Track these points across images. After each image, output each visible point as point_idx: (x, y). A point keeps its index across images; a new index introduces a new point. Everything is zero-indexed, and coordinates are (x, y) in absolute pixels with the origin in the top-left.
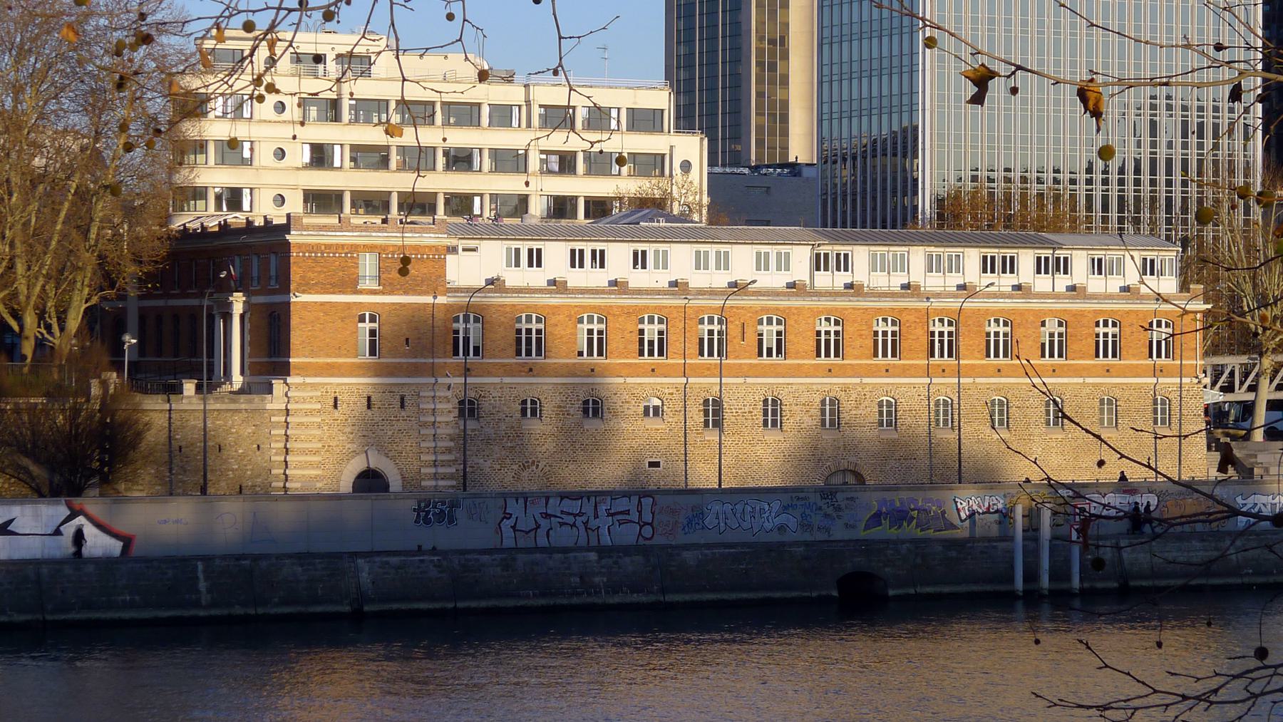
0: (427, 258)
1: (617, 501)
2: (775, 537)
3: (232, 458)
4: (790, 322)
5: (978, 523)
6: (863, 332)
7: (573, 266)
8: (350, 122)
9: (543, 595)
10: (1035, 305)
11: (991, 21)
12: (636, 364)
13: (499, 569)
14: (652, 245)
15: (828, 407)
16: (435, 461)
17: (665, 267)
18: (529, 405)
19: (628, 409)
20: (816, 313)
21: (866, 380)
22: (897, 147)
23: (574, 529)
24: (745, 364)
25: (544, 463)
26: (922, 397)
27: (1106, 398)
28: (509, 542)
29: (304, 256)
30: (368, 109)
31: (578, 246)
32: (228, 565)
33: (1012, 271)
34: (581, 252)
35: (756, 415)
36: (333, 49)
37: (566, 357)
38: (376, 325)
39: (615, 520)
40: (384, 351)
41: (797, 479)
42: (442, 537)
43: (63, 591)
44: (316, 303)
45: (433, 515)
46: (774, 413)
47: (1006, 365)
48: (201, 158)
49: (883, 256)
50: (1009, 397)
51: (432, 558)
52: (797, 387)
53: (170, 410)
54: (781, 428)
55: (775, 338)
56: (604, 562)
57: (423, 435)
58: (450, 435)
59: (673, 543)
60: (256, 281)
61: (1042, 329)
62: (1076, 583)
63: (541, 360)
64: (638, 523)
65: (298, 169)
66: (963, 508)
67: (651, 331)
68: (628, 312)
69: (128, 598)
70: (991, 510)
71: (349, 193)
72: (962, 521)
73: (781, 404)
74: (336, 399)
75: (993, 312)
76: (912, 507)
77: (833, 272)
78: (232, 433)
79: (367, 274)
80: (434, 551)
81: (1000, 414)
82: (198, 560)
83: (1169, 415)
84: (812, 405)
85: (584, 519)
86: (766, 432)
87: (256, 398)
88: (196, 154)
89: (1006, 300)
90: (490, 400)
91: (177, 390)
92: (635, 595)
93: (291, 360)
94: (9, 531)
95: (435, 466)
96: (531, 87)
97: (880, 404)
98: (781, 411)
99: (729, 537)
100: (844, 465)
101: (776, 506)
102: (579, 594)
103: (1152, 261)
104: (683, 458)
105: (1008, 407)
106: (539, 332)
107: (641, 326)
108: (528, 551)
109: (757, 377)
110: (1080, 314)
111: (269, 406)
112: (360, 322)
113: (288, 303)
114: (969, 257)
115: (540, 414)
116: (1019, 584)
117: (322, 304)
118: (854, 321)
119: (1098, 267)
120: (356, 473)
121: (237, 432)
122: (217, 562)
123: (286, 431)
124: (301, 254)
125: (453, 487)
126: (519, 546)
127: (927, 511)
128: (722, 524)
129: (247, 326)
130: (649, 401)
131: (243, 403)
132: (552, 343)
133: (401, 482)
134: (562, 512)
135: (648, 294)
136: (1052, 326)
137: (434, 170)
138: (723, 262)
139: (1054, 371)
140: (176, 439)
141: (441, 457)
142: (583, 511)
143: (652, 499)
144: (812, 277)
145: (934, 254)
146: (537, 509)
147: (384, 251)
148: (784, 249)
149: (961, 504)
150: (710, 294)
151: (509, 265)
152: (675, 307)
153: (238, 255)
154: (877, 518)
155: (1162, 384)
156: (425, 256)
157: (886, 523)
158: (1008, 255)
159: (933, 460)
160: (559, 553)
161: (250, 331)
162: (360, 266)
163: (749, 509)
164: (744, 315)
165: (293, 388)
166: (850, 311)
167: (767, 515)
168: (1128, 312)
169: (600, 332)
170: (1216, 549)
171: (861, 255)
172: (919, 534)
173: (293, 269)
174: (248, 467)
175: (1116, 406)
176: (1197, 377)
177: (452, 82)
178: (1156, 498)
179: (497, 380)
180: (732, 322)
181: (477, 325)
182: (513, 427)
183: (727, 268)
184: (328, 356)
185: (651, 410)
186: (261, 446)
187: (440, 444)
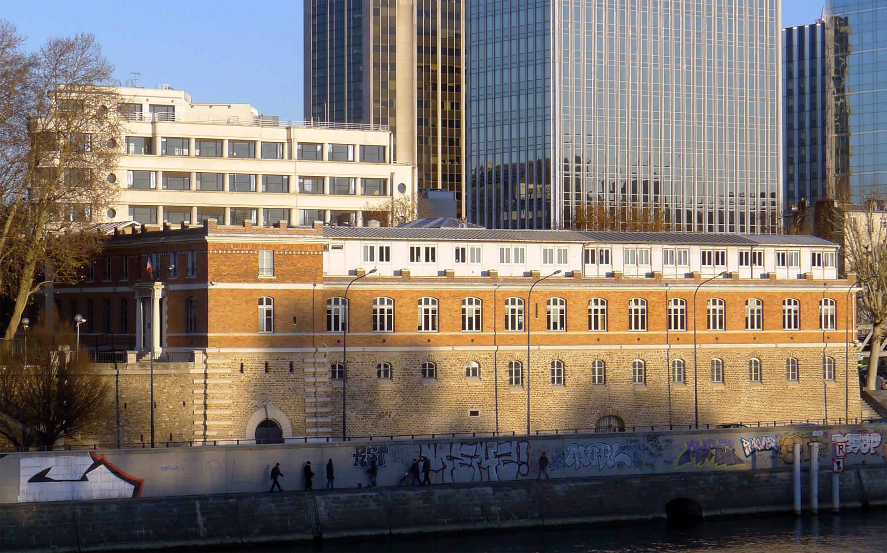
0: (309, 254)
1: (502, 445)
2: (615, 472)
3: (164, 413)
4: (570, 303)
5: (758, 459)
6: (621, 310)
7: (545, 262)
8: (162, 155)
9: (454, 522)
10: (742, 289)
11: (600, 84)
12: (460, 336)
14: (469, 244)
15: (597, 368)
18: (382, 368)
19: (455, 370)
21: (625, 347)
22: (492, 179)
23: (471, 468)
24: (538, 335)
25: (395, 413)
26: (664, 359)
27: (790, 358)
29: (218, 253)
30: (175, 145)
31: (416, 245)
32: (219, 504)
33: (723, 263)
34: (418, 249)
35: (546, 374)
36: (147, 100)
37: (410, 331)
39: (500, 460)
40: (277, 327)
41: (576, 423)
43: (93, 528)
44: (227, 289)
46: (559, 372)
47: (722, 334)
49: (633, 252)
50: (724, 359)
51: (371, 494)
53: (117, 375)
55: (559, 315)
56: (497, 494)
58: (325, 392)
60: (191, 272)
61: (746, 306)
62: (837, 504)
63: (391, 333)
66: (748, 446)
68: (454, 295)
69: (144, 532)
70: (767, 448)
71: (329, 211)
73: (564, 366)
74: (242, 365)
75: (712, 294)
76: (712, 446)
77: (598, 264)
79: (265, 267)
82: (195, 499)
83: (834, 371)
84: (587, 366)
85: (478, 460)
87: (182, 365)
89: (721, 285)
90: (355, 365)
91: (123, 359)
92: (522, 521)
93: (208, 335)
94: (47, 478)
95: (316, 417)
96: (292, 129)
97: (634, 365)
98: (564, 370)
99: (582, 473)
100: (610, 412)
101: (616, 447)
102: (480, 521)
103: (819, 255)
104: (495, 408)
105: (723, 366)
106: (389, 311)
107: (463, 307)
109: (547, 345)
110: (772, 296)
111: (192, 371)
112: (259, 304)
113: (206, 290)
114: (693, 252)
115: (391, 375)
116: (798, 506)
117: (232, 290)
118: (615, 302)
119: (782, 260)
120: (258, 423)
121: (168, 392)
122: (211, 501)
123: (205, 391)
125: (329, 433)
127: (722, 450)
128: (578, 463)
129: (165, 308)
131: (172, 368)
132: (399, 320)
133: (291, 429)
134: (462, 455)
135: (468, 282)
136: (753, 305)
137: (189, 189)
138: (520, 257)
139: (755, 338)
140: (123, 398)
141: (320, 410)
143: (527, 444)
144: (583, 268)
145: (669, 250)
146: (443, 454)
147: (277, 248)
149: (746, 443)
150: (513, 282)
152: (488, 292)
153: (155, 253)
154: (687, 455)
155: (829, 348)
156: (307, 253)
158: (707, 251)
159: (672, 407)
160: (464, 488)
161: (168, 313)
162: (259, 260)
164: (537, 298)
165: (210, 357)
166: (613, 294)
167: (609, 454)
168: (805, 294)
169: (434, 311)
171: (617, 251)
172: (717, 468)
173: (210, 263)
175: (798, 365)
176: (853, 342)
177: (236, 125)
178: (880, 436)
179: (360, 349)
182: (371, 386)
183: (523, 261)
185: (471, 371)
186: (186, 403)
187: (320, 399)
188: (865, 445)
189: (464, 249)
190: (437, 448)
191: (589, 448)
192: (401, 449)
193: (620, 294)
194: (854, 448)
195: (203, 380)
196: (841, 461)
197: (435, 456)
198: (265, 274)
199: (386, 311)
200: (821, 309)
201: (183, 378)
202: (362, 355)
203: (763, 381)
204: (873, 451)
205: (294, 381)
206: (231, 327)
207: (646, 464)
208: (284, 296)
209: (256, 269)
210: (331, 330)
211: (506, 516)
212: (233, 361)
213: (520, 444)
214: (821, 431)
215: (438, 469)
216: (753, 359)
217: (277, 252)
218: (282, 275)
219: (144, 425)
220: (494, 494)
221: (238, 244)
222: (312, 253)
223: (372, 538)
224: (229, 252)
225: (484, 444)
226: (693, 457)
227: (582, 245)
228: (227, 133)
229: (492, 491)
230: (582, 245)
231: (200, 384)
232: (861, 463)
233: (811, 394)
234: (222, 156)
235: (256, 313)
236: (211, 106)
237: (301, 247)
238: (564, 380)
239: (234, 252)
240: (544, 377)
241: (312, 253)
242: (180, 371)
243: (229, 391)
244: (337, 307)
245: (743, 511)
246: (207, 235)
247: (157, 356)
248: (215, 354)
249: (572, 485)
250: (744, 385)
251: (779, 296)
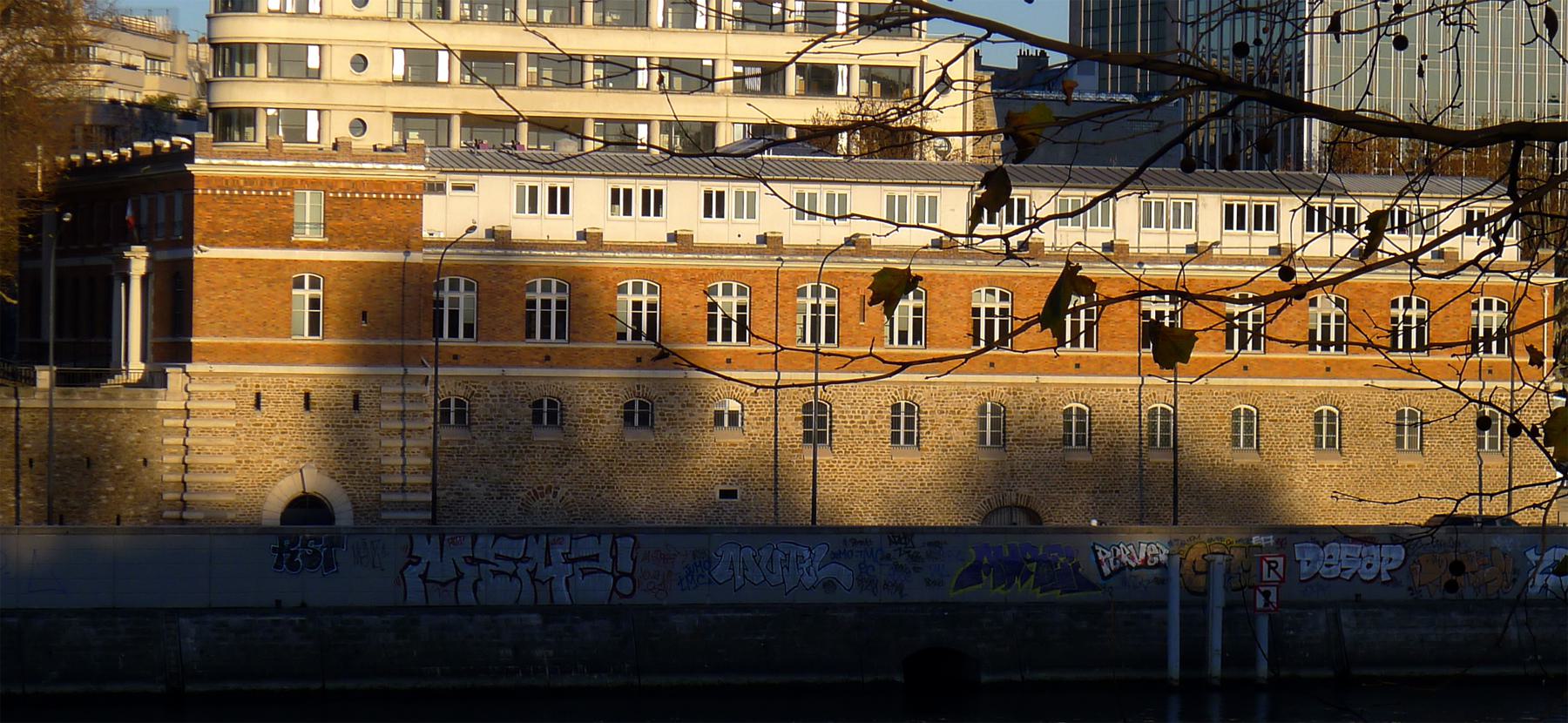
1: (580, 541)
3: (107, 477)
7: (708, 214)
16: (404, 484)
17: (752, 215)
19: (691, 415)
20: (972, 283)
23: (516, 581)
25: (566, 490)
26: (1131, 405)
27: (1406, 409)
28: (415, 597)
31: (623, 184)
33: (1270, 227)
39: (576, 568)
41: (940, 517)
44: (230, 260)
45: (302, 557)
46: (909, 423)
47: (1256, 360)
48: (249, 68)
52: (942, 387)
53: (18, 408)
54: (918, 445)
57: (386, 448)
59: (665, 603)
61: (1311, 309)
64: (612, 573)
65: (385, 84)
67: (728, 303)
68: (691, 277)
70: (1149, 564)
71: (658, 123)
74: (258, 395)
76: (1029, 557)
78: (106, 442)
79: (308, 221)
80: (303, 608)
88: (553, 80)
93: (192, 340)
101: (821, 553)
105: (1258, 420)
106: (652, 306)
111: (160, 404)
114: (1205, 205)
116: (1174, 669)
117: (240, 262)
118: (1029, 295)
124: (209, 192)
126: (431, 604)
127: (1051, 564)
134: (497, 556)
139: (1328, 369)
140: (25, 449)
142: (529, 555)
148: (928, 192)
149: (1104, 554)
151: (520, 209)
152: (762, 272)
154: (973, 573)
156: (392, 196)
157: (988, 580)
162: (295, 210)
163: (780, 555)
166: (1023, 280)
167: (805, 566)
174: (130, 490)
178: (1403, 551)
180: (847, 294)
182: (520, 439)
184: (247, 334)
185: (726, 417)
186: (150, 460)
188: (1369, 566)
189: (661, 191)
190: (445, 543)
191: (763, 552)
192: (372, 542)
193: (1039, 281)
194: (1342, 570)
195: (183, 421)
196: (1273, 590)
197: (442, 557)
198: (309, 234)
199: (983, 313)
200: (1478, 317)
201: (144, 416)
202: (503, 383)
203: (1344, 450)
204: (1386, 577)
205: (361, 426)
206: (238, 327)
208: (344, 274)
209: (288, 223)
210: (457, 337)
212: (242, 388)
213: (618, 540)
214: (1271, 537)
215: (444, 580)
216: (1325, 408)
217: (331, 195)
219: (65, 498)
221: (255, 178)
222: (400, 196)
224: (236, 192)
226: (987, 574)
227: (969, 189)
229: (540, 622)
230: (969, 189)
231: (177, 427)
232: (1354, 598)
233: (1447, 477)
234: (581, 24)
235: (287, 302)
237: (379, 185)
238: (918, 438)
239: (245, 193)
240: (876, 432)
241: (400, 196)
242: (138, 404)
243: (231, 442)
246: (193, 162)
247: (135, 377)
248: (204, 374)
250: (1300, 455)
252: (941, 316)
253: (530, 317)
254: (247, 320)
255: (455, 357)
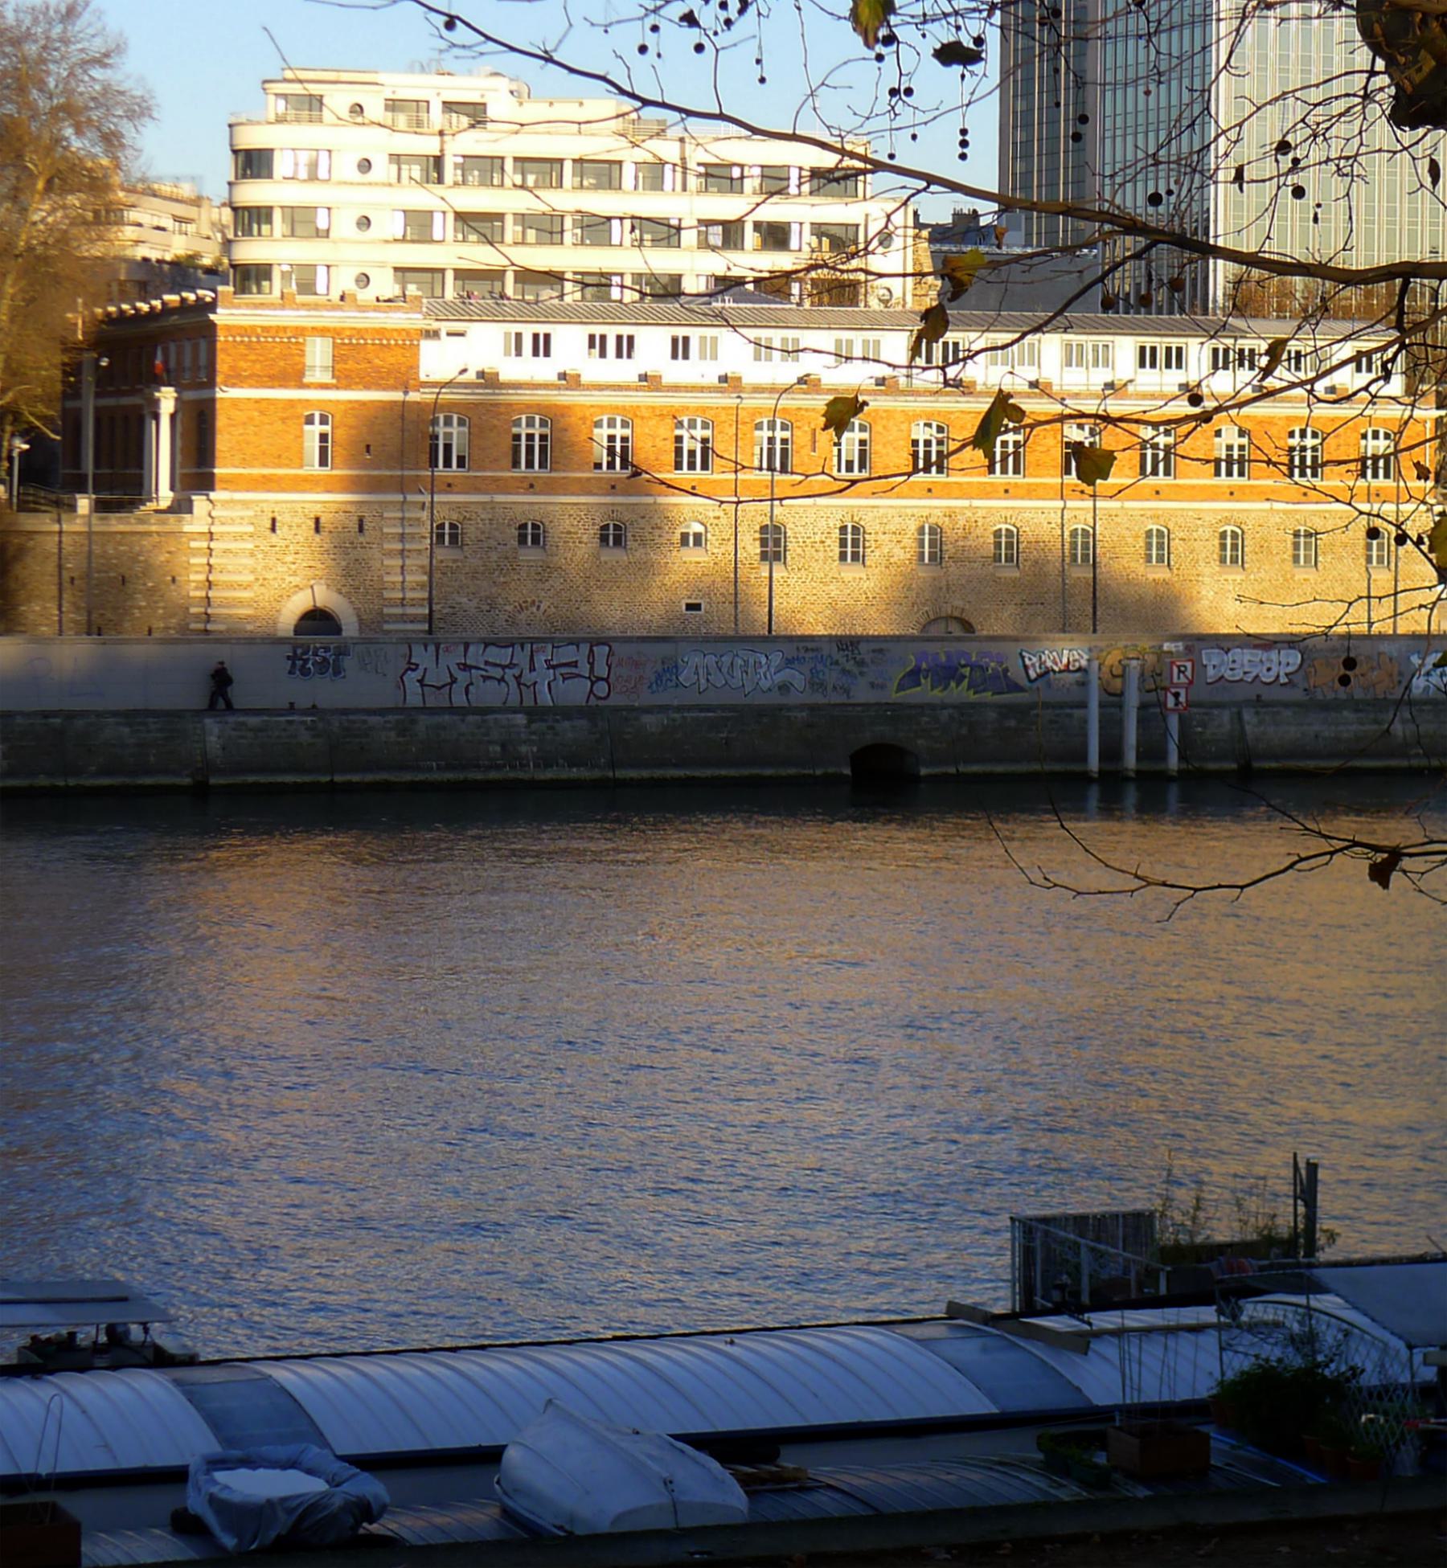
2: (776, 699)
4: (877, 428)
7: (674, 356)
9: (450, 767)
13: (393, 734)
15: (927, 537)
20: (911, 418)
21: (976, 503)
28: (414, 700)
30: (488, 168)
33: (1179, 366)
38: (327, 428)
40: (337, 460)
42: (325, 692)
46: (855, 543)
50: (1171, 527)
53: (60, 533)
55: (857, 448)
56: (534, 726)
61: (1217, 440)
62: (1173, 762)
65: (387, 242)
68: (661, 414)
72: (1031, 681)
74: (274, 521)
76: (963, 662)
80: (314, 710)
81: (1159, 545)
86: (845, 567)
93: (216, 471)
99: (711, 699)
100: (947, 610)
101: (777, 659)
102: (498, 768)
104: (732, 598)
106: (624, 439)
107: (678, 432)
108: (433, 711)
111: (187, 528)
113: (212, 401)
116: (1094, 763)
117: (257, 401)
127: (983, 669)
128: (703, 681)
130: (688, 527)
134: (487, 663)
151: (507, 353)
152: (724, 408)
154: (914, 676)
163: (740, 662)
170: (1376, 722)
173: (221, 357)
181: (462, 429)
184: (264, 465)
188: (1269, 669)
196: (1183, 692)
199: (537, 438)
204: (1283, 680)
207: (835, 688)
211: (546, 762)
218: (347, 377)
220: (527, 726)
223: (298, 788)
225: (528, 647)
228: (567, 146)
236: (551, 104)
242: (167, 528)
243: (250, 562)
244: (448, 430)
245: (1000, 768)
246: (214, 312)
247: (164, 504)
249: (677, 716)
251: (1281, 423)
252: (884, 445)
253: (516, 450)
254: (264, 453)
255: (449, 485)
